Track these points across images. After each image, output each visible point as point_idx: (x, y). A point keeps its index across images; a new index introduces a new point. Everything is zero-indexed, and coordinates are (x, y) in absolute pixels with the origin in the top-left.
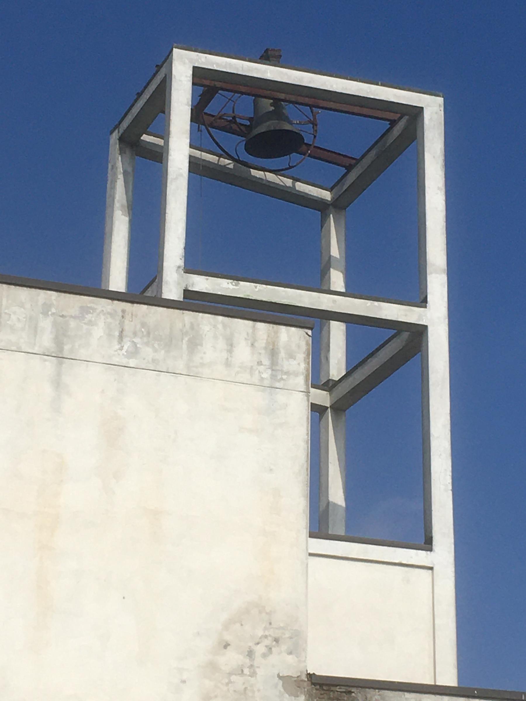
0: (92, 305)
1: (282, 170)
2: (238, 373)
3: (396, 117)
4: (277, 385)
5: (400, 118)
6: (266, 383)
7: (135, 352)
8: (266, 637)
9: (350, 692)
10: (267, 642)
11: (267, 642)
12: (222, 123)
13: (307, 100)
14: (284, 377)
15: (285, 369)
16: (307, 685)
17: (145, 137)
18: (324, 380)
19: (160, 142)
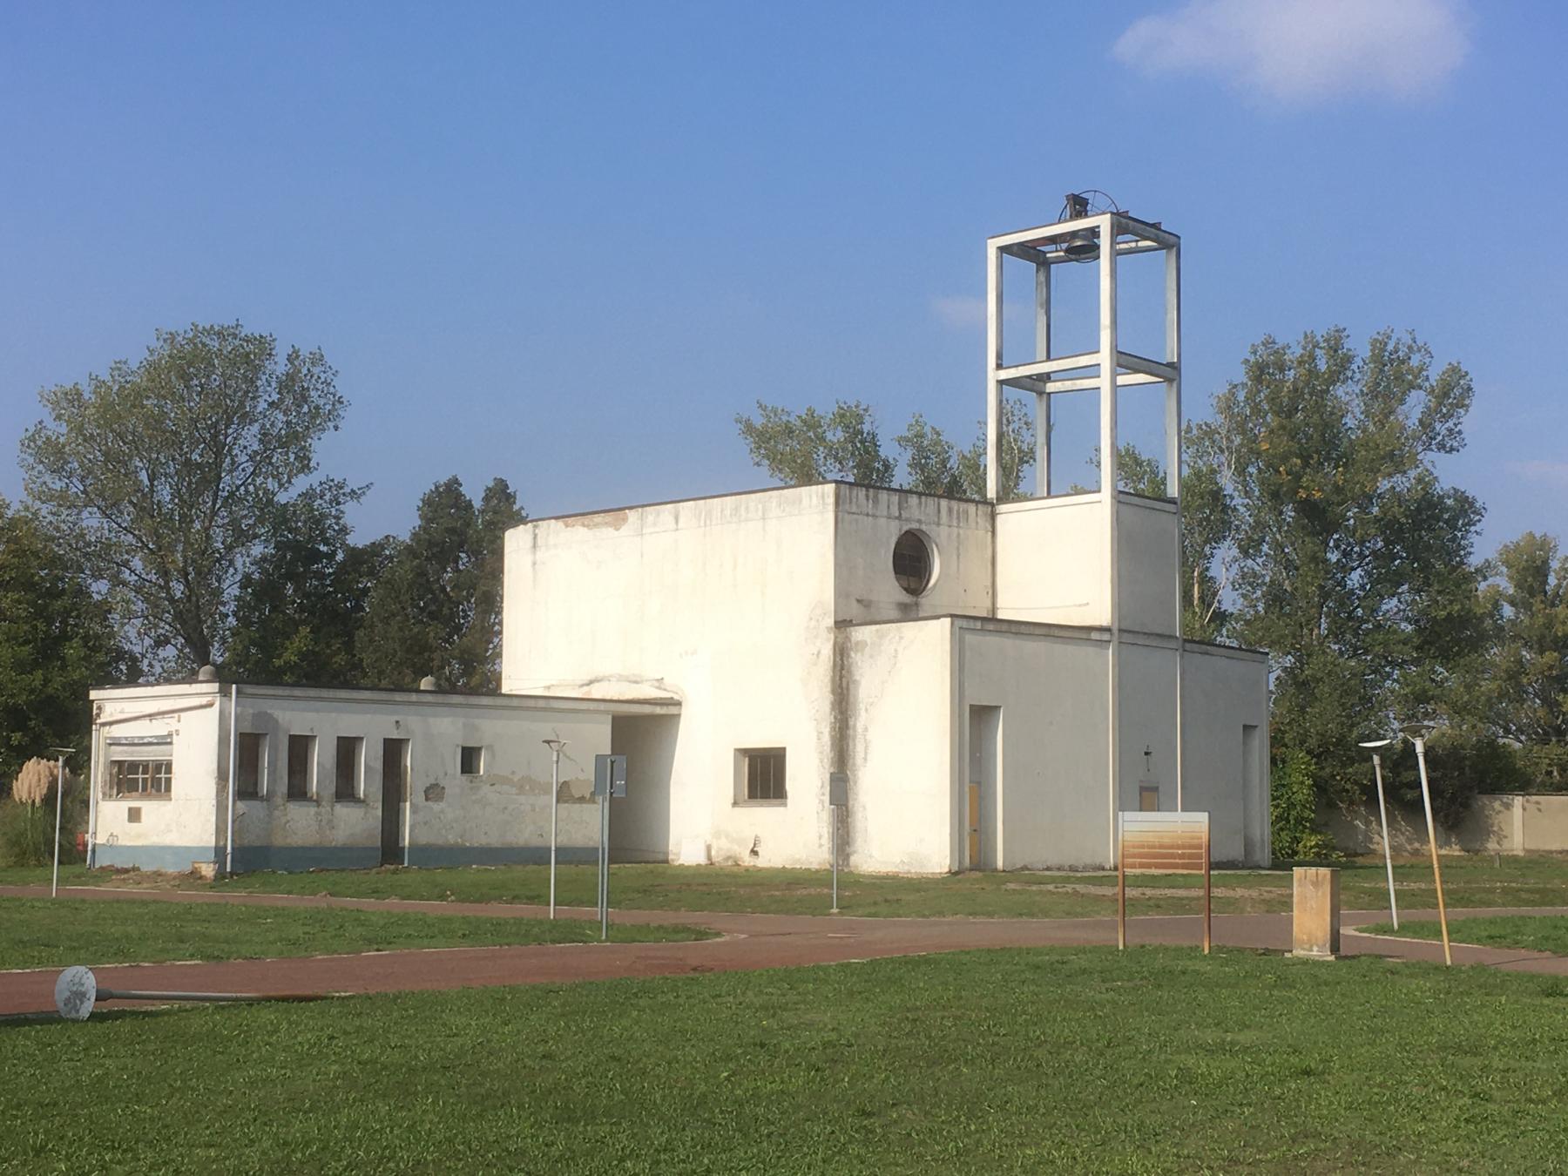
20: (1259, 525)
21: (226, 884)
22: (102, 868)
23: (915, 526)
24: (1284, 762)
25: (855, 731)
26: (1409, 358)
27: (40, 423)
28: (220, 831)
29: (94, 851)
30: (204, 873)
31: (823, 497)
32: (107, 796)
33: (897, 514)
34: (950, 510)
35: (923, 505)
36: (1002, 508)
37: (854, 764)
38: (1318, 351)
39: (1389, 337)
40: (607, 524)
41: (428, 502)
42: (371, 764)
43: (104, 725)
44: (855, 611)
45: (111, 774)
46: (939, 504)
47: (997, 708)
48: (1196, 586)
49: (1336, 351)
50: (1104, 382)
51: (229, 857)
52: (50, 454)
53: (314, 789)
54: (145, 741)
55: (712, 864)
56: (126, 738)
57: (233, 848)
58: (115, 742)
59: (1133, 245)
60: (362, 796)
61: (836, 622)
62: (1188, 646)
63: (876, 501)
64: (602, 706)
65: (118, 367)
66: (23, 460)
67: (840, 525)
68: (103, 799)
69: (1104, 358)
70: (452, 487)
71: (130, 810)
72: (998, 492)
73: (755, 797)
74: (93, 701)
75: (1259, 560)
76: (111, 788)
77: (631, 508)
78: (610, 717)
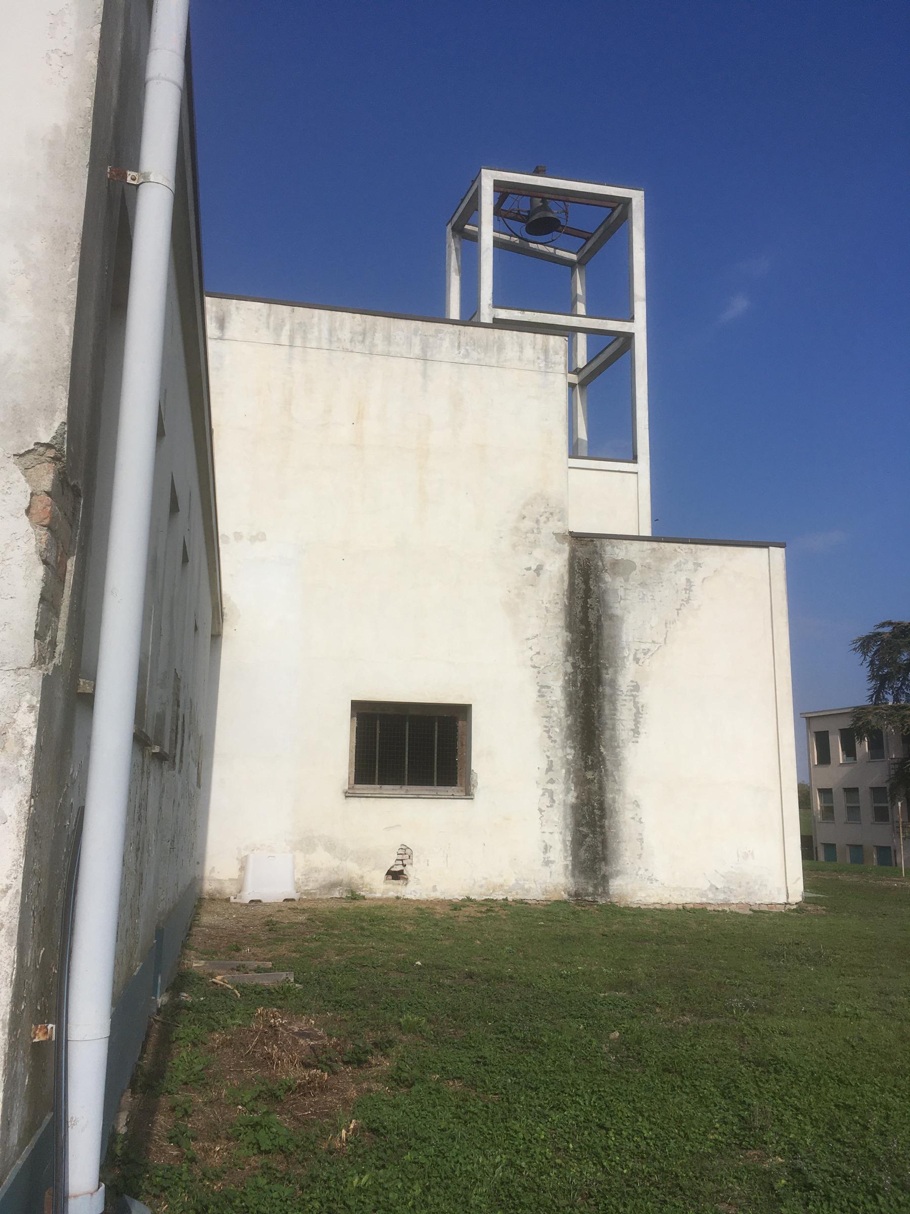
0: (442, 328)
1: (548, 242)
2: (526, 364)
3: (615, 205)
4: (548, 371)
5: (618, 206)
6: (543, 369)
7: (467, 355)
8: (546, 512)
9: (593, 541)
10: (546, 515)
11: (546, 515)
12: (512, 215)
13: (561, 198)
14: (553, 365)
15: (553, 361)
16: (569, 538)
17: (467, 227)
18: (574, 368)
19: (476, 229)
29: (887, 736)
37: (613, 738)
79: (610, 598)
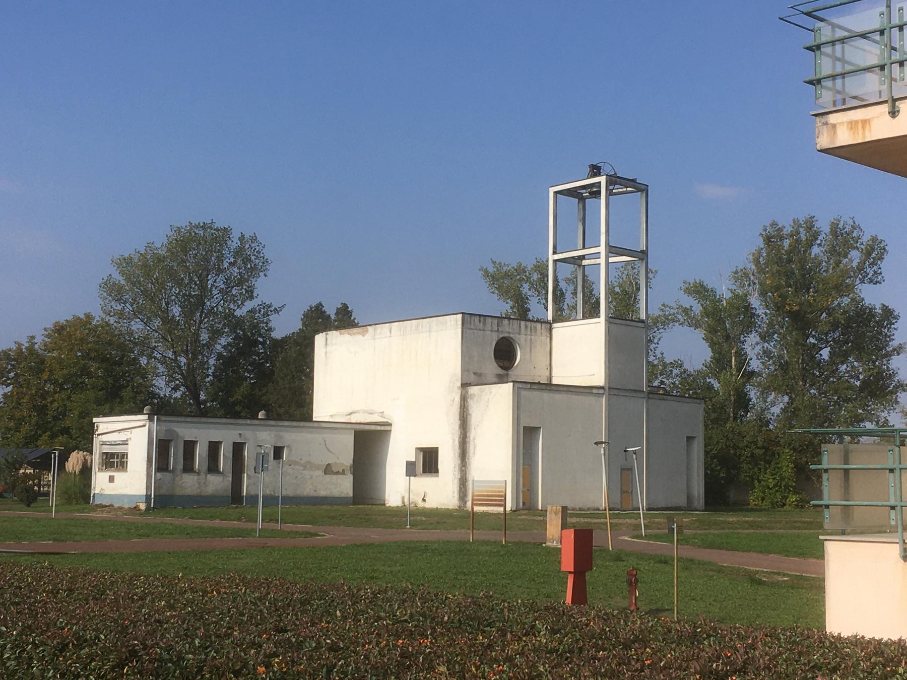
20: (771, 325)
21: (150, 513)
22: (96, 505)
23: (506, 335)
24: (779, 455)
25: (469, 438)
26: (853, 232)
27: (110, 275)
28: (148, 487)
29: (94, 496)
30: (141, 508)
31: (456, 320)
32: (100, 470)
33: (496, 329)
34: (526, 327)
35: (511, 324)
36: (555, 325)
37: (469, 456)
38: (801, 230)
39: (839, 221)
40: (359, 333)
41: (306, 315)
42: (227, 454)
43: (99, 435)
44: (472, 378)
45: (102, 459)
46: (520, 324)
47: (540, 428)
48: (733, 358)
49: (810, 229)
50: (602, 261)
51: (152, 500)
52: (113, 290)
53: (197, 467)
54: (117, 443)
55: (405, 506)
56: (109, 441)
57: (154, 495)
58: (104, 444)
59: (625, 189)
60: (221, 470)
61: (462, 384)
62: (651, 396)
63: (484, 324)
64: (349, 426)
65: (149, 246)
66: (101, 294)
67: (464, 335)
68: (99, 472)
69: (602, 249)
70: (319, 306)
71: (110, 476)
72: (553, 317)
73: (426, 472)
74: (94, 423)
75: (772, 344)
76: (102, 466)
77: (370, 325)
78: (353, 431)
79: (469, 408)
